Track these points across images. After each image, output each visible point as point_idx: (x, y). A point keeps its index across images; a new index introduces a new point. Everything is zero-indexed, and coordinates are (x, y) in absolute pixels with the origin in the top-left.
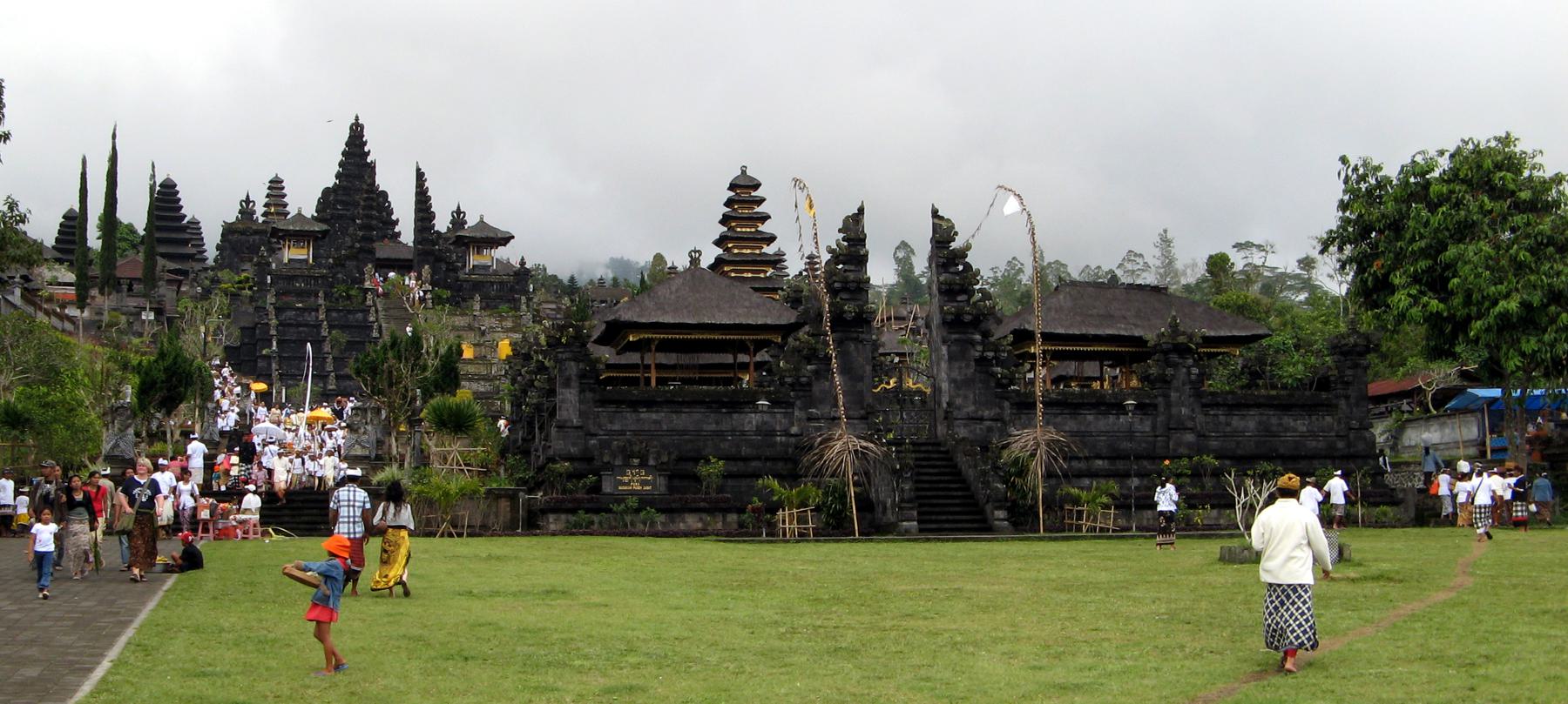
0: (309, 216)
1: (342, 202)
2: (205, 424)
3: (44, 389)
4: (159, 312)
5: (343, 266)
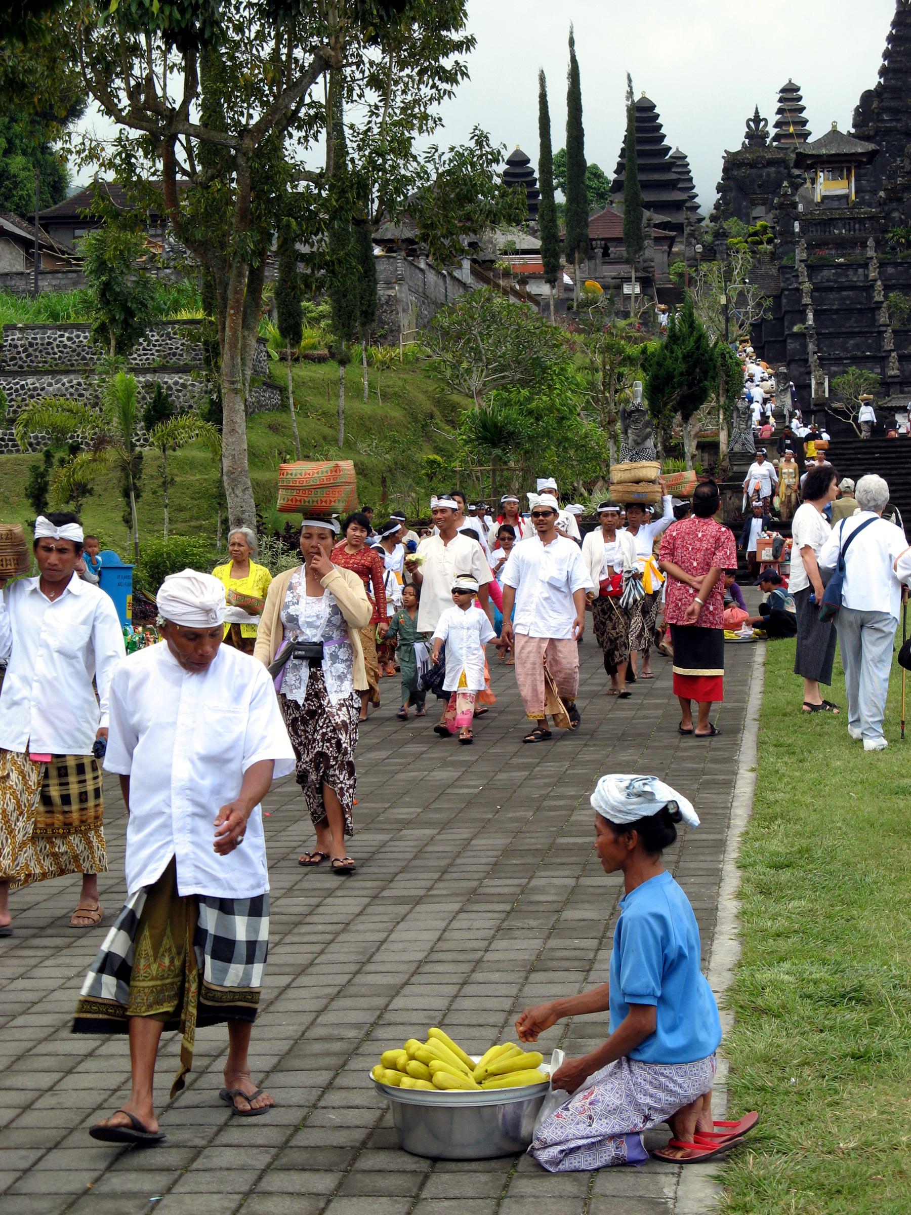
0: (845, 133)
1: (888, 110)
2: (735, 431)
3: (525, 392)
4: (646, 282)
5: (900, 200)
